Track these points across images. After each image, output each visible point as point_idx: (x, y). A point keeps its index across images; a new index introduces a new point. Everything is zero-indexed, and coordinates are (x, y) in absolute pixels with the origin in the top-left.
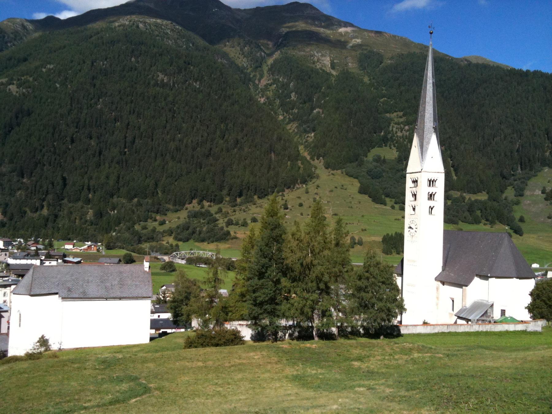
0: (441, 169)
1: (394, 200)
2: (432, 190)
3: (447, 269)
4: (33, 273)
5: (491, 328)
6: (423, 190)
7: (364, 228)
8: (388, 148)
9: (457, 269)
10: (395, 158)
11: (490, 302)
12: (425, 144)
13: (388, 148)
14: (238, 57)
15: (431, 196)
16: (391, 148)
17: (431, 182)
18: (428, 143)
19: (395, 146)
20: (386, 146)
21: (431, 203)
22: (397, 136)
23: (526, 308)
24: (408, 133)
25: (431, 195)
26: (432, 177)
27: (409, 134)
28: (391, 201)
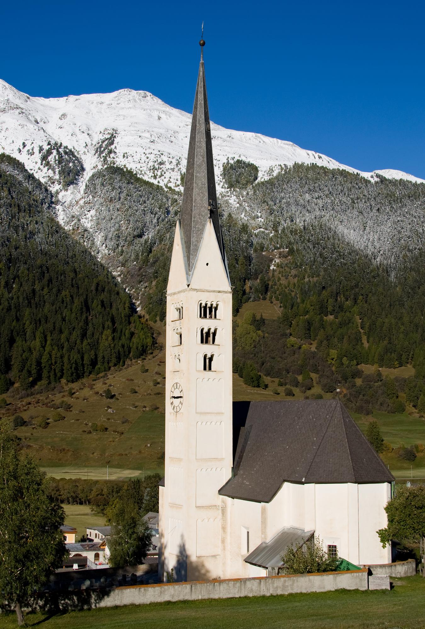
0: (226, 286)
1: (277, 380)
2: (208, 324)
3: (241, 472)
4: (260, 579)
5: (284, 587)
6: (195, 324)
7: (83, 410)
8: (267, 302)
9: (255, 471)
10: (279, 318)
11: (308, 528)
12: (193, 240)
13: (267, 302)
14: (39, 169)
15: (207, 337)
16: (272, 303)
17: (208, 311)
18: (199, 240)
19: (277, 299)
20: (264, 299)
21: (208, 349)
22: (281, 284)
23: (377, 532)
24: (296, 280)
25: (208, 333)
26: (208, 299)
27: (298, 281)
28: (273, 381)
